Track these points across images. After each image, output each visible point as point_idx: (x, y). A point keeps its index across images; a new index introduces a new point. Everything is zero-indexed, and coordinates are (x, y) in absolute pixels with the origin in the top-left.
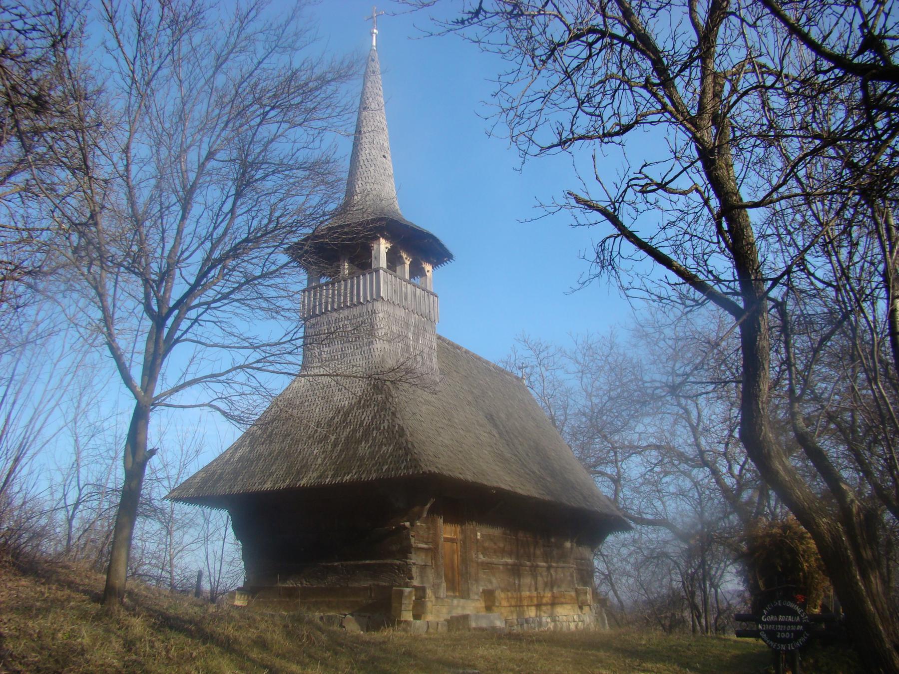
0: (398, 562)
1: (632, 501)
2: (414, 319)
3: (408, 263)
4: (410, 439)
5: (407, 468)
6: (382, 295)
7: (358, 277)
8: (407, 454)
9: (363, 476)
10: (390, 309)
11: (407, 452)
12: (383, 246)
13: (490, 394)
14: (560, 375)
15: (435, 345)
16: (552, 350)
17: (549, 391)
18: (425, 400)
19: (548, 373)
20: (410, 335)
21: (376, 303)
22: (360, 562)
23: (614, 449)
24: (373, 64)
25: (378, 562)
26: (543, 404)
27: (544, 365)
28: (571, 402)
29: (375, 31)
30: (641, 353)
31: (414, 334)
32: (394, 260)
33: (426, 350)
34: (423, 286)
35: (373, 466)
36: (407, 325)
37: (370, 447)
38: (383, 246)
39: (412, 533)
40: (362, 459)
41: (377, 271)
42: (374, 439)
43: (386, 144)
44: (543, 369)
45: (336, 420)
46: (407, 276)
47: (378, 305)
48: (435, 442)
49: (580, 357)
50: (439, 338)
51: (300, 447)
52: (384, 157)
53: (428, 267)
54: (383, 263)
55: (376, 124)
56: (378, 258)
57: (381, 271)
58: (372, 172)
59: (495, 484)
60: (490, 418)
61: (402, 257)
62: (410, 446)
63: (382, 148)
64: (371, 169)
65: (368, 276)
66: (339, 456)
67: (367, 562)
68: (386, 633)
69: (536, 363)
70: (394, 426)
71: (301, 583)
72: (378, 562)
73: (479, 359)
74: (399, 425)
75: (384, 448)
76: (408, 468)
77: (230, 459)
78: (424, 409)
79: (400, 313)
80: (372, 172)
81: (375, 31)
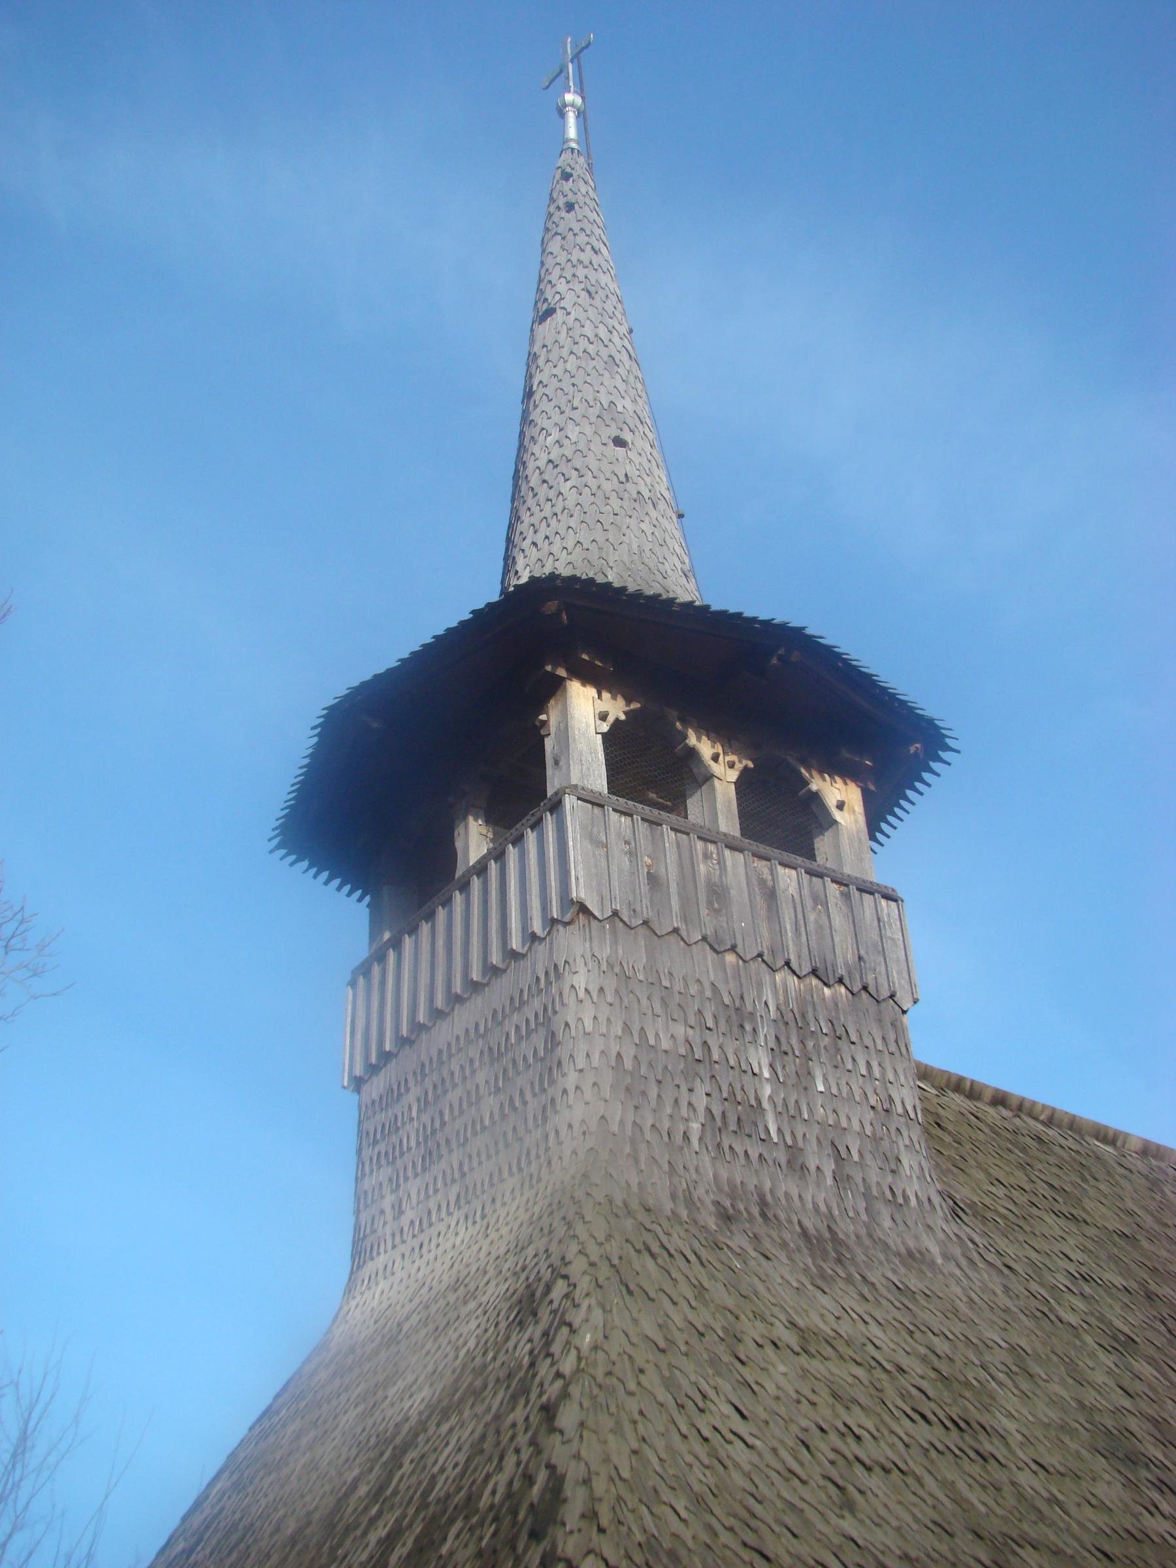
3: (733, 775)
12: (585, 714)
15: (906, 1096)
20: (760, 1059)
24: (567, 186)
31: (779, 1052)
32: (647, 770)
36: (739, 1019)
38: (585, 714)
41: (556, 806)
46: (728, 823)
47: (572, 943)
50: (924, 1073)
52: (619, 442)
53: (841, 797)
61: (693, 753)
64: (565, 488)
73: (267, 1413)
80: (572, 497)
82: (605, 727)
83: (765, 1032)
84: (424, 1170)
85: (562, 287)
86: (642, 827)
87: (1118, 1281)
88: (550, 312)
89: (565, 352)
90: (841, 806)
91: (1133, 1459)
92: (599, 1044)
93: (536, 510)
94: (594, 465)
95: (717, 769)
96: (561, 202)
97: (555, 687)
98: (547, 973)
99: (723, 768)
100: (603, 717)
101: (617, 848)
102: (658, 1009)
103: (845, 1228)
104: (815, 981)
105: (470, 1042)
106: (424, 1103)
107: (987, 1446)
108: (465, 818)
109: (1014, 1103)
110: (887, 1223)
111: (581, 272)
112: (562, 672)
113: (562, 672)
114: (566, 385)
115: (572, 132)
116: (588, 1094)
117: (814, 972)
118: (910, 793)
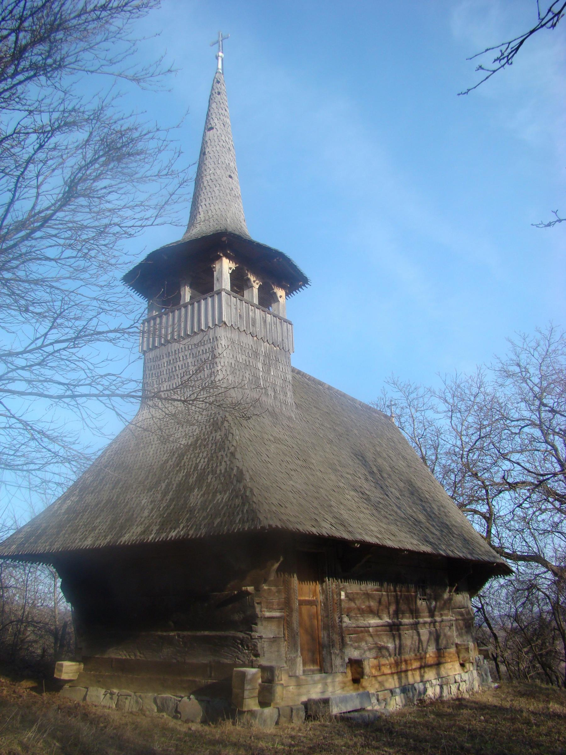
0: (241, 635)
1: (508, 539)
2: (264, 347)
3: (257, 287)
4: (249, 485)
5: (242, 521)
6: (224, 319)
7: (199, 302)
8: (243, 504)
9: (191, 532)
10: (235, 336)
11: (245, 500)
12: (226, 267)
13: (356, 432)
14: (430, 415)
15: (289, 377)
16: (421, 391)
17: (419, 431)
18: (275, 438)
19: (418, 414)
20: (260, 366)
21: (218, 329)
22: (199, 633)
23: (485, 487)
24: (218, 86)
25: (218, 633)
26: (414, 444)
27: (414, 407)
28: (442, 442)
29: (220, 54)
30: (507, 392)
32: (239, 284)
33: (279, 382)
34: (276, 313)
35: (205, 518)
36: (256, 354)
37: (203, 495)
38: (226, 267)
39: (257, 600)
40: (191, 511)
41: (219, 293)
42: (209, 485)
43: (232, 164)
44: (413, 411)
45: (170, 463)
46: (256, 301)
47: (221, 332)
48: (283, 487)
49: (449, 396)
50: (293, 370)
51: (128, 496)
52: (230, 177)
53: (280, 292)
54: (226, 283)
55: (221, 143)
56: (220, 280)
57: (223, 293)
58: (217, 192)
59: (359, 537)
60: (361, 457)
61: (249, 280)
62: (248, 493)
63: (228, 167)
64: (215, 189)
65: (210, 300)
66: (168, 506)
67: (206, 633)
68: (228, 726)
69: (406, 404)
70: (232, 469)
71: (135, 655)
72: (218, 633)
73: (344, 395)
74: (238, 468)
75: (219, 497)
76: (244, 522)
77: (57, 510)
78: (272, 448)
79: (248, 340)
80: (217, 192)
81: (220, 54)
82: (230, 272)
83: (262, 358)
84: (168, 381)
85: (216, 121)
86: (238, 301)
87: (328, 426)
88: (212, 128)
89: (216, 144)
90: (281, 297)
91: (337, 470)
92: (227, 360)
93: (206, 193)
94: (224, 184)
95: (255, 284)
96: (216, 91)
97: (219, 258)
98: (213, 338)
99: (256, 284)
100: (230, 269)
101: (233, 307)
102: (240, 351)
103: (277, 410)
104: (273, 346)
105: (186, 350)
106: (169, 363)
107: (311, 466)
108: (185, 286)
109: (302, 374)
110: (284, 409)
111: (222, 117)
112: (221, 255)
113: (221, 255)
114: (216, 154)
115: (220, 66)
116: (224, 372)
117: (273, 343)
118: (294, 292)
